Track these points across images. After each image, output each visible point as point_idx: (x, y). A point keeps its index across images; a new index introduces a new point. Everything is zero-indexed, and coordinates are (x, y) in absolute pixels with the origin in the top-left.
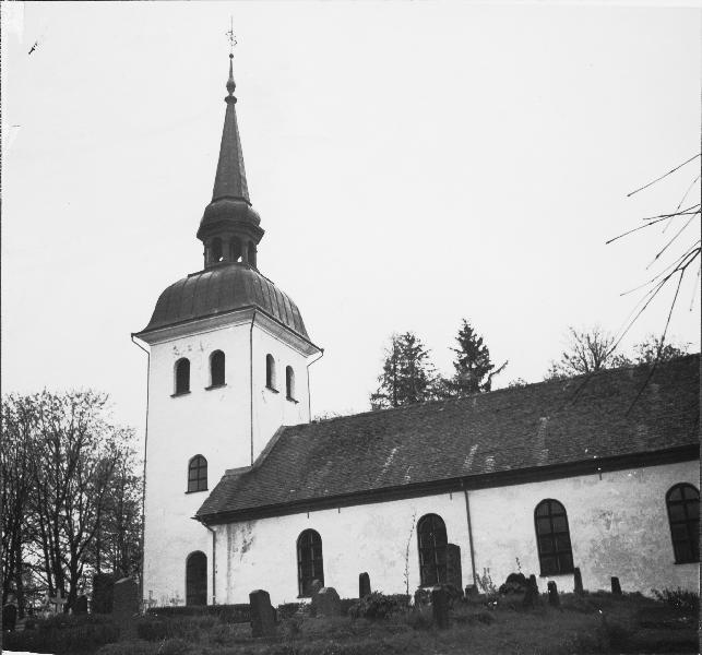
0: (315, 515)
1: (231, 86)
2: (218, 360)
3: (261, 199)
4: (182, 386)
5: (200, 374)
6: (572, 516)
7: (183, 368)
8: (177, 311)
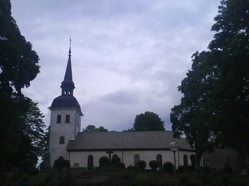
1: (70, 52)
5: (63, 119)
7: (59, 117)
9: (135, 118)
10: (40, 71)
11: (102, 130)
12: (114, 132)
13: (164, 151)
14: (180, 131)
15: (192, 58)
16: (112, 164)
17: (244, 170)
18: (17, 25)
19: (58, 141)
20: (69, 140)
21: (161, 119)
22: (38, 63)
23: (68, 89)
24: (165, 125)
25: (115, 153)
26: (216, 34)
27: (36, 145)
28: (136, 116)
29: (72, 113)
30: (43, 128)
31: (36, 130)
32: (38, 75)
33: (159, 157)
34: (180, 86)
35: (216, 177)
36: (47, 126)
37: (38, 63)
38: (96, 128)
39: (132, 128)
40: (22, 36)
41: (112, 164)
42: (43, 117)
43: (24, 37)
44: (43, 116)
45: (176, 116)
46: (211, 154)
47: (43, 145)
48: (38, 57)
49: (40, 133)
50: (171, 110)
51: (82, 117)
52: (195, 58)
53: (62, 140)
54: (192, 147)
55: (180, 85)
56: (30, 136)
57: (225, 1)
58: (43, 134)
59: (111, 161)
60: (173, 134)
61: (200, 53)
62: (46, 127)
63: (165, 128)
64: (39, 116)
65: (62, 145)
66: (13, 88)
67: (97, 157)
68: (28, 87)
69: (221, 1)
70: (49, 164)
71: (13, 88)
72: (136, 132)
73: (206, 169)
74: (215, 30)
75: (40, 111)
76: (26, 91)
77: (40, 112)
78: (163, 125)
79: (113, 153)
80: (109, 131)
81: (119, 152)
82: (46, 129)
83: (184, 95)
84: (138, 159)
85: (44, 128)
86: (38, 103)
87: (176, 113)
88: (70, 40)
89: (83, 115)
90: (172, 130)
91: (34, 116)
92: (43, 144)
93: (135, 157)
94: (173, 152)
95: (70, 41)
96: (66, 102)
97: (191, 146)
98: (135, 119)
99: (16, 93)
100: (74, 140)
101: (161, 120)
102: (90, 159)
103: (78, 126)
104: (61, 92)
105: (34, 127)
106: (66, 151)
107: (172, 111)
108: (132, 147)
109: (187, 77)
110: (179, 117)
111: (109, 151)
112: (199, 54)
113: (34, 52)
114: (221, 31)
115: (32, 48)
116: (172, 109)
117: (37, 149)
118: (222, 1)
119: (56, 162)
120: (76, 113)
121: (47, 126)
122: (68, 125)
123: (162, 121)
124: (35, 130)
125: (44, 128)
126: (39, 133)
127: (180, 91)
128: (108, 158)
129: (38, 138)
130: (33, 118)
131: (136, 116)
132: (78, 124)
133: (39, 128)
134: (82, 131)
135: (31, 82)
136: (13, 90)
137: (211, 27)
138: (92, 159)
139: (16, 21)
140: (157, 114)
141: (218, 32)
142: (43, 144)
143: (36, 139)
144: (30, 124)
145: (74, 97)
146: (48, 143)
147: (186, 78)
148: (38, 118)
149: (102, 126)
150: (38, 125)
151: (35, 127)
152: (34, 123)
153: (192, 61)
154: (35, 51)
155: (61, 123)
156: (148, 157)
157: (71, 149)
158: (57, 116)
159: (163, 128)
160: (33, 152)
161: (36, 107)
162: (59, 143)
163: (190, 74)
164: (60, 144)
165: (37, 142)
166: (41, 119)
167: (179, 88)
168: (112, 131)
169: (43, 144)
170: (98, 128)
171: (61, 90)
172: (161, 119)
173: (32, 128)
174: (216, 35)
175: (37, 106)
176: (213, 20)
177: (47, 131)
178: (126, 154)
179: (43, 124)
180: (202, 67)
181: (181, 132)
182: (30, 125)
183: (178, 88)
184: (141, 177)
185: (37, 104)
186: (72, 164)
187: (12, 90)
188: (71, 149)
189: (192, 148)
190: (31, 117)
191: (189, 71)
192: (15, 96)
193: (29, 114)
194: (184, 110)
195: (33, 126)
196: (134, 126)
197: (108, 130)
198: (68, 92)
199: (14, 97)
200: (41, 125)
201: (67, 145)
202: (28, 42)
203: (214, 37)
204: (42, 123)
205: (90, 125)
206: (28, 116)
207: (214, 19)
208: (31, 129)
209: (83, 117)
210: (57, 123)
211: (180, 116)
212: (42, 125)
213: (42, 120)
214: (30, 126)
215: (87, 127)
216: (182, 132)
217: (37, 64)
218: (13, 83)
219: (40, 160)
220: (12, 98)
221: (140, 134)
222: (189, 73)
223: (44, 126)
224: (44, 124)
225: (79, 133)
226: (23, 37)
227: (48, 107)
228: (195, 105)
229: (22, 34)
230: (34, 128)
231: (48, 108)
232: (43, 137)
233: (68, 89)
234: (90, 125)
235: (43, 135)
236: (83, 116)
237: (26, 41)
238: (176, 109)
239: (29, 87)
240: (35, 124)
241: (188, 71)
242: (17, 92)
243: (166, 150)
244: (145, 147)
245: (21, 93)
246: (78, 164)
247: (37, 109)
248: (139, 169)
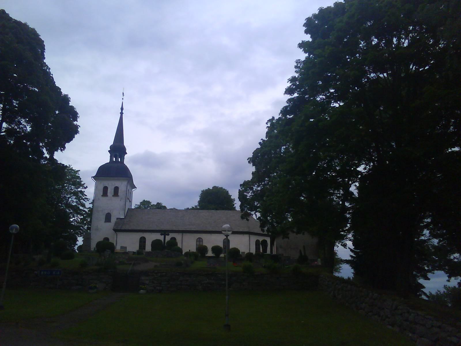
1: (122, 109)
2: (116, 189)
5: (110, 191)
7: (105, 189)
9: (200, 194)
10: (79, 132)
11: (159, 206)
12: (174, 210)
13: (237, 235)
14: (249, 212)
15: (266, 125)
16: (167, 248)
17: (319, 260)
18: (51, 73)
19: (103, 217)
20: (117, 218)
21: (231, 195)
22: (77, 121)
23: (118, 154)
24: (236, 204)
25: (172, 235)
26: (289, 99)
27: (75, 222)
28: (202, 191)
29: (122, 185)
30: (84, 202)
31: (76, 204)
32: (76, 136)
33: (227, 242)
34: (251, 158)
35: (286, 267)
36: (89, 199)
37: (77, 121)
38: (151, 204)
39: (196, 205)
40: (57, 87)
41: (167, 248)
42: (86, 188)
43: (60, 88)
44: (85, 186)
45: (246, 194)
46: (286, 240)
47: (85, 223)
48: (77, 114)
49: (81, 208)
50: (240, 186)
51: (135, 190)
52: (270, 125)
53: (108, 217)
54: (263, 231)
55: (251, 155)
56: (68, 211)
57: (300, 61)
58: (85, 209)
59: (166, 245)
60: (240, 214)
61: (277, 119)
62: (89, 201)
63: (235, 207)
64: (80, 186)
65: (108, 224)
66: (44, 151)
67: (150, 238)
68: (63, 151)
69: (296, 60)
70: (90, 246)
71: (44, 151)
72: (200, 211)
73: (275, 258)
74: (289, 94)
75: (81, 180)
76: (58, 156)
77: (82, 181)
78: (233, 203)
79: (168, 235)
80: (168, 208)
81: (177, 234)
82: (90, 204)
83: (255, 169)
84: (201, 244)
85: (86, 202)
86: (80, 171)
87: (246, 190)
88: (123, 93)
89: (136, 188)
90: (240, 210)
91: (74, 187)
92: (85, 222)
93: (197, 241)
94: (225, 236)
95: (123, 95)
96: (115, 170)
97: (261, 229)
98: (201, 195)
99: (47, 157)
100: (124, 218)
101: (232, 197)
102: (143, 241)
103: (128, 201)
104: (110, 158)
105: (73, 201)
107: (240, 187)
108: (193, 228)
109: (259, 147)
110: (249, 195)
111: (165, 233)
112: (275, 120)
113: (72, 107)
114: (296, 95)
115: (70, 102)
116: (241, 185)
117: (77, 228)
118: (297, 60)
119: (99, 244)
120: (127, 184)
121: (90, 200)
123: (233, 198)
124: (74, 204)
125: (86, 202)
126: (79, 208)
127: (250, 164)
128: (162, 242)
129: (78, 213)
130: (73, 188)
131: (202, 191)
133: (80, 202)
134: (135, 207)
135: (67, 145)
136: (45, 154)
137: (285, 90)
138: (145, 242)
139: (50, 68)
140: (227, 190)
141: (291, 97)
142: (85, 221)
143: (75, 215)
144: (69, 196)
145: (125, 164)
146: (91, 221)
147: (258, 148)
148: (79, 190)
149: (160, 202)
150: (78, 198)
151: (75, 200)
152: (73, 196)
153: (267, 128)
154: (74, 107)
156: (218, 240)
157: (119, 228)
159: (234, 207)
160: (72, 231)
161: (76, 175)
162: (104, 221)
163: (263, 144)
165: (77, 219)
166: (83, 190)
167: (249, 160)
168: (173, 208)
169: (85, 222)
170: (154, 205)
171: (110, 156)
172: (231, 195)
173: (71, 201)
174: (289, 101)
175: (78, 174)
176: (287, 82)
177: (91, 206)
178: (187, 236)
179: (85, 197)
180: (277, 137)
181: (250, 213)
182: (69, 198)
183: (248, 159)
184: (200, 264)
185: (78, 172)
186: (118, 248)
187: (43, 154)
188: (119, 229)
189: (263, 232)
190: (69, 188)
191: (262, 139)
192: (46, 162)
193: (67, 183)
194: (255, 186)
195: (72, 199)
196: (199, 204)
197: (167, 207)
198: (118, 159)
199: (45, 162)
200: (82, 198)
201: (114, 225)
202: (66, 95)
203: (286, 102)
204: (84, 196)
205: (144, 200)
206: (66, 186)
207: (288, 81)
208: (70, 202)
209: (136, 190)
210: (102, 196)
211: (250, 194)
212: (84, 198)
213: (84, 191)
214: (69, 199)
215: (141, 202)
216: (251, 213)
217: (75, 123)
218: (44, 144)
219: (80, 241)
220: (42, 163)
221: (205, 213)
222: (263, 142)
223: (86, 199)
224: (86, 197)
225: (130, 210)
226: (59, 88)
227: (92, 176)
228: (269, 181)
229: (57, 84)
230: (73, 201)
231: (92, 177)
232: (84, 213)
233: (118, 154)
234: (144, 200)
235: (84, 211)
236: (136, 189)
237: (63, 93)
238: (246, 185)
239: (64, 151)
240: (75, 197)
241: (261, 140)
242: (48, 157)
243: (262, 236)
244: (211, 229)
245: (54, 158)
246: (126, 248)
247: (79, 178)
248: (200, 255)
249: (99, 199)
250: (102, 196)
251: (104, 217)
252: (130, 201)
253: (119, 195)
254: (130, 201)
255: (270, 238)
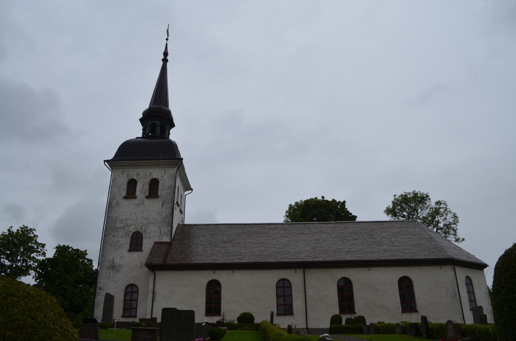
0: (217, 272)
1: (166, 54)
2: (154, 184)
3: (175, 106)
4: (131, 194)
5: (142, 188)
6: (356, 287)
7: (132, 184)
8: (127, 155)
19: (126, 242)
29: (163, 175)
89: (192, 190)
95: (168, 33)
106: (146, 269)
122: (155, 205)
132: (179, 203)
138: (219, 293)
155: (135, 197)
158: (126, 181)
162: (128, 248)
164: (130, 251)
231: (105, 161)
249: (118, 204)
250: (125, 198)
251: (128, 240)
252: (181, 211)
253: (159, 194)
254: (181, 211)
255: (282, 224)
